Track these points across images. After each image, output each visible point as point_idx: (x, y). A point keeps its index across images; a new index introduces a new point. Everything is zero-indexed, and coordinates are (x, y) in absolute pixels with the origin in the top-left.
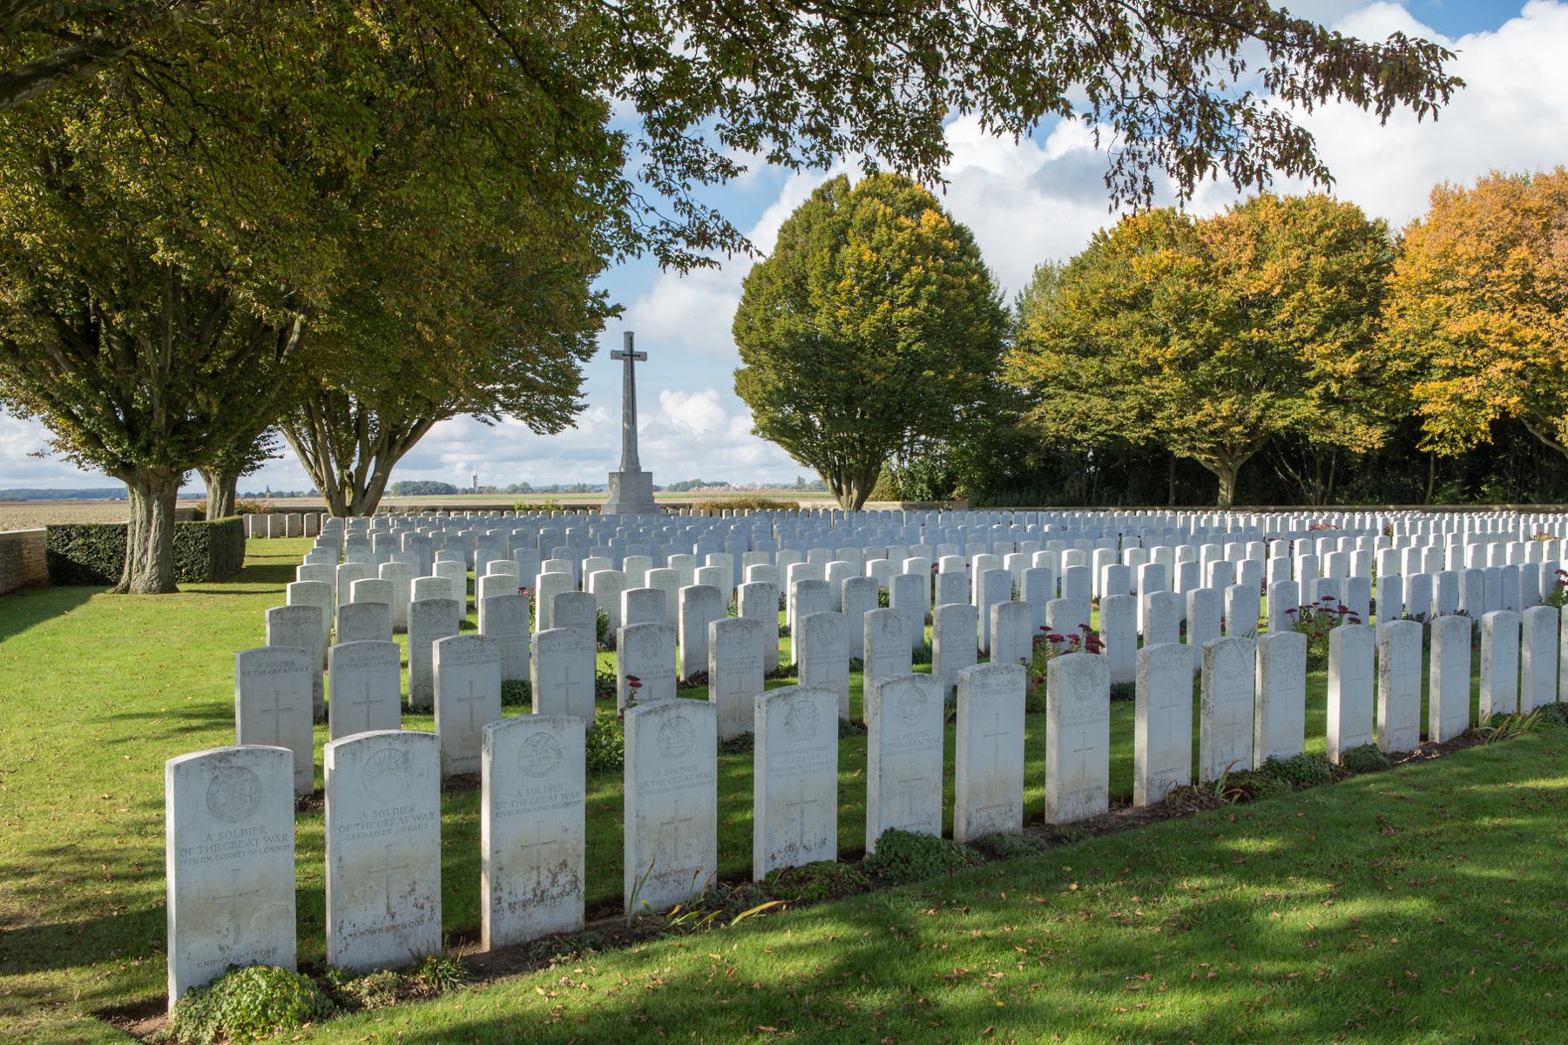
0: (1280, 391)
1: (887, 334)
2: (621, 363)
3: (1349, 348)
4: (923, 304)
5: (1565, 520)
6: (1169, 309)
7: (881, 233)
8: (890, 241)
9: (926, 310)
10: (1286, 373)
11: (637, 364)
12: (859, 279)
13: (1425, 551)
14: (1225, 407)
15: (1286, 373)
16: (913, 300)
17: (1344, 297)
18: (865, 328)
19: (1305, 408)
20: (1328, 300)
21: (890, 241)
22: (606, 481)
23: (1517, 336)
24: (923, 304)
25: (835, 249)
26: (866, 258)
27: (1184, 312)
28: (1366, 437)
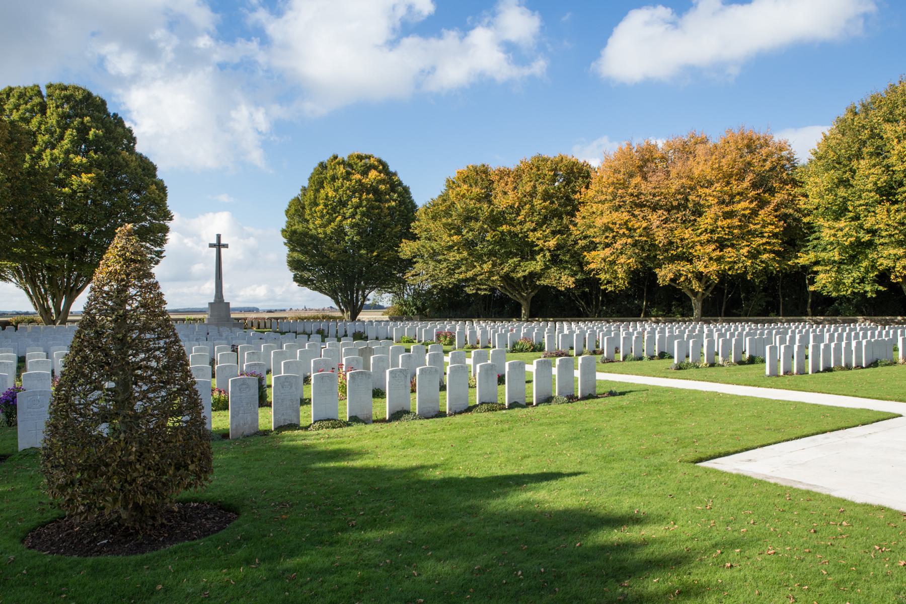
0: (523, 258)
1: (340, 232)
2: (214, 249)
3: (554, 233)
4: (358, 217)
5: (904, 329)
6: (459, 215)
7: (338, 183)
8: (342, 186)
9: (360, 220)
10: (527, 251)
11: (223, 250)
12: (326, 206)
13: (833, 345)
14: (487, 267)
15: (527, 251)
16: (353, 216)
17: (555, 206)
18: (329, 230)
19: (536, 265)
20: (545, 208)
21: (342, 186)
22: (207, 306)
23: (630, 225)
24: (358, 217)
25: (317, 191)
26: (330, 195)
27: (468, 217)
28: (566, 281)
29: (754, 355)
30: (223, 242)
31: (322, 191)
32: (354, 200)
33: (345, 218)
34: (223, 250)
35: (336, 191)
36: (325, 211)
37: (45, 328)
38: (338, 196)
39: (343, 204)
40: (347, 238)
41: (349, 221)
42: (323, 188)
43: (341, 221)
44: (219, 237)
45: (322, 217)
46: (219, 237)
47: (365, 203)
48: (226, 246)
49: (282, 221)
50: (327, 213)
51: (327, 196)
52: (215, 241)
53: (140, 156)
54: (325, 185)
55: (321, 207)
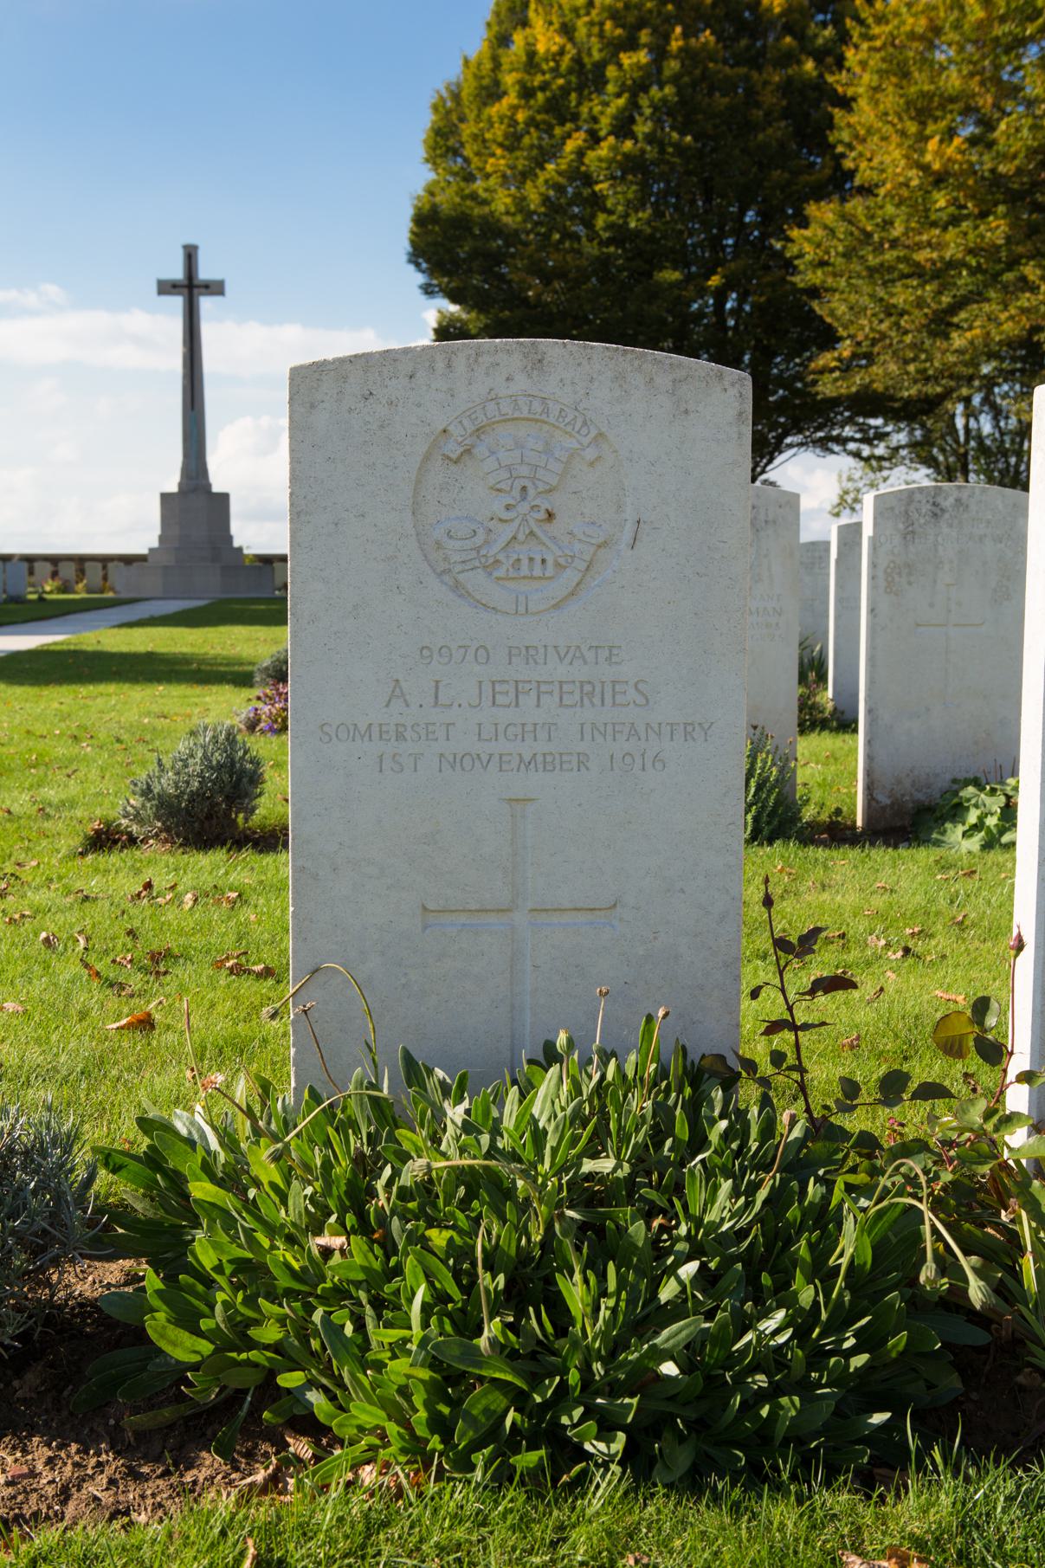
1: (578, 191)
4: (642, 128)
11: (206, 304)
12: (527, 93)
16: (623, 127)
18: (533, 194)
26: (541, 48)
29: (840, 708)
30: (204, 273)
31: (518, 38)
32: (627, 59)
33: (595, 139)
34: (206, 304)
35: (567, 30)
36: (521, 116)
37: (983, 491)
38: (571, 51)
39: (589, 78)
40: (601, 220)
41: (604, 150)
42: (525, 23)
43: (580, 153)
44: (190, 255)
45: (512, 142)
46: (190, 255)
47: (673, 66)
48: (215, 288)
49: (410, 178)
50: (531, 122)
51: (531, 54)
52: (177, 273)
53: (736, 363)
54: (531, 14)
55: (512, 99)
